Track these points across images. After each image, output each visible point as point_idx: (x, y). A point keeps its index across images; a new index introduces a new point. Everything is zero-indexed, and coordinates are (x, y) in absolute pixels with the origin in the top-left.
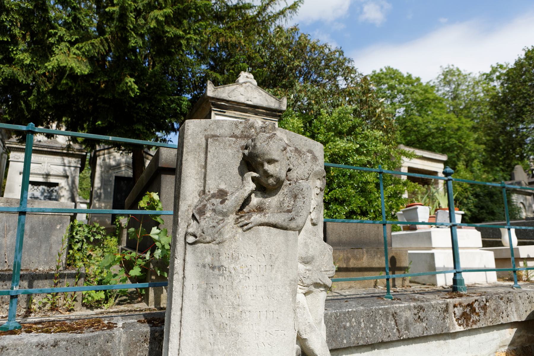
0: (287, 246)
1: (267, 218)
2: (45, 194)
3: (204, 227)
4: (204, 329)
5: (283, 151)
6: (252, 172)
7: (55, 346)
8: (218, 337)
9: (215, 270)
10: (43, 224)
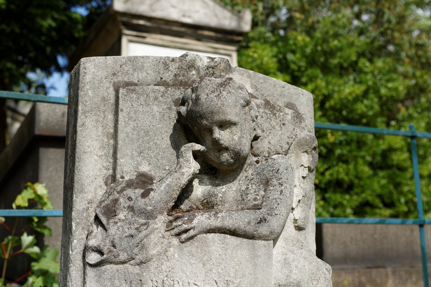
0: (255, 265)
3: (116, 237)
5: (244, 107)
6: (194, 144)
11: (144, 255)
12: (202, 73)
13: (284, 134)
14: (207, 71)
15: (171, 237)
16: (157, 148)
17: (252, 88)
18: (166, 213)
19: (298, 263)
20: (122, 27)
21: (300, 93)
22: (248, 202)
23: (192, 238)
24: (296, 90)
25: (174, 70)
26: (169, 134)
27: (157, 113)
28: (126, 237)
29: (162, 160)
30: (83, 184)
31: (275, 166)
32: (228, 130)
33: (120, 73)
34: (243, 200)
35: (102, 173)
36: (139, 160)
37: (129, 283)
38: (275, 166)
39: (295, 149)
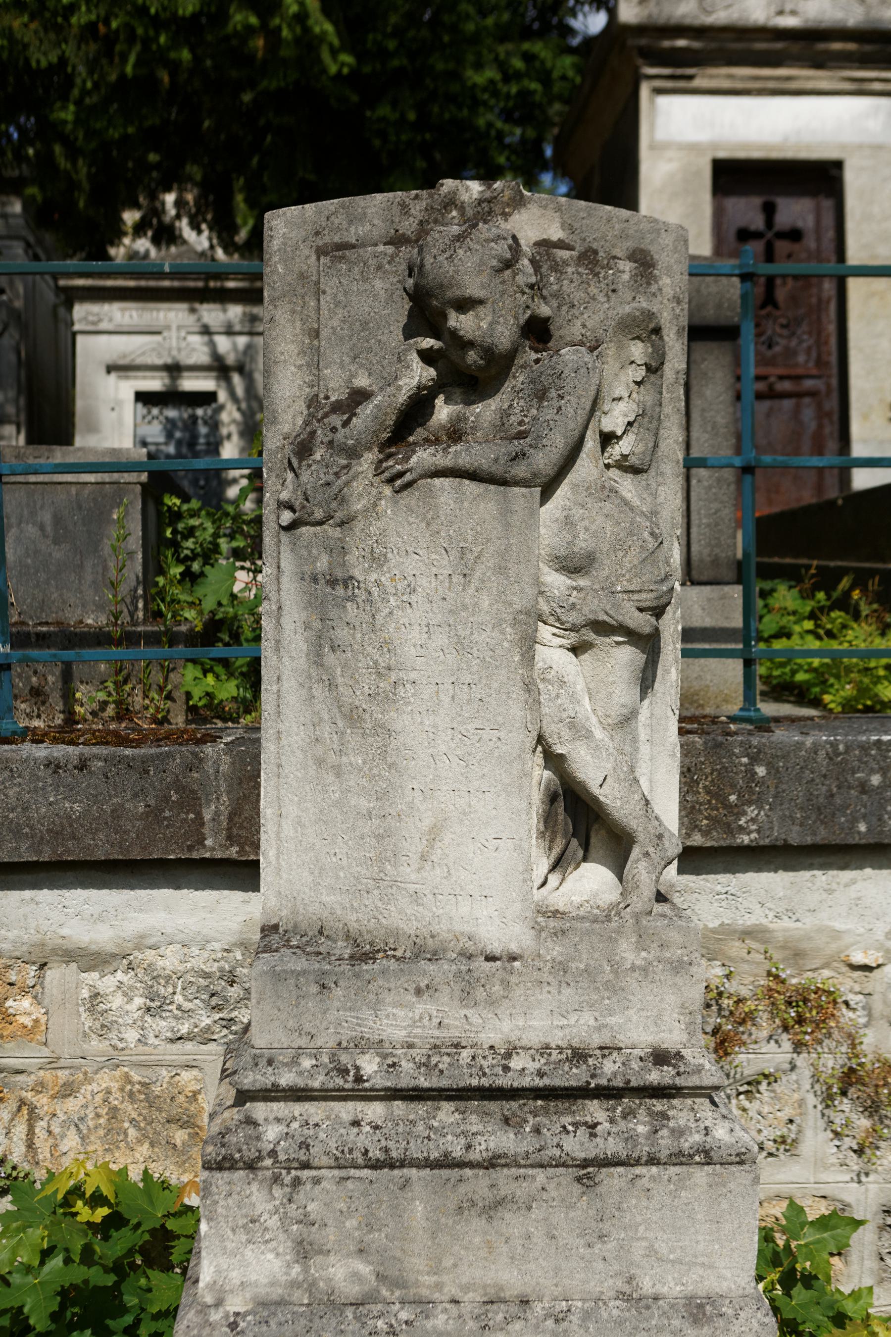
0: (508, 525)
1: (450, 457)
2: (178, 434)
4: (321, 720)
5: (499, 271)
6: (419, 339)
7: (82, 770)
9: (338, 588)
10: (80, 507)
12: (470, 212)
14: (479, 209)
18: (376, 449)
19: (591, 523)
20: (640, 61)
23: (409, 485)
26: (401, 325)
27: (382, 292)
34: (503, 424)
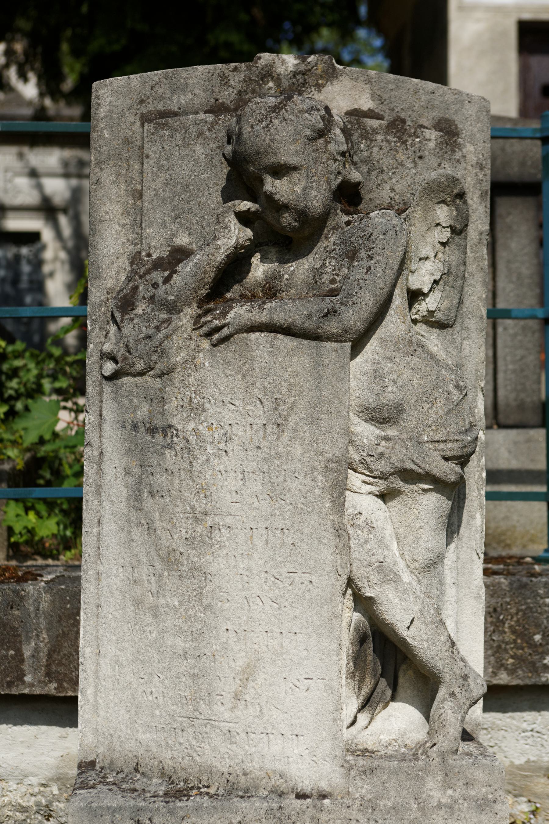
0: (320, 378)
1: (265, 313)
3: (130, 339)
4: (139, 562)
5: (312, 140)
6: (237, 202)
8: (165, 580)
9: (157, 435)
11: (165, 364)
12: (285, 84)
13: (421, 174)
15: (199, 338)
16: (201, 210)
17: (373, 101)
18: (195, 305)
21: (464, 100)
22: (322, 286)
23: (226, 339)
24: (456, 96)
25: (237, 85)
26: (220, 187)
27: (202, 157)
28: (143, 338)
29: (208, 227)
30: (100, 266)
31: (368, 229)
32: (286, 178)
33: (151, 98)
34: (316, 283)
35: (126, 250)
36: (174, 229)
37: (149, 401)
38: (368, 229)
39: (421, 200)
